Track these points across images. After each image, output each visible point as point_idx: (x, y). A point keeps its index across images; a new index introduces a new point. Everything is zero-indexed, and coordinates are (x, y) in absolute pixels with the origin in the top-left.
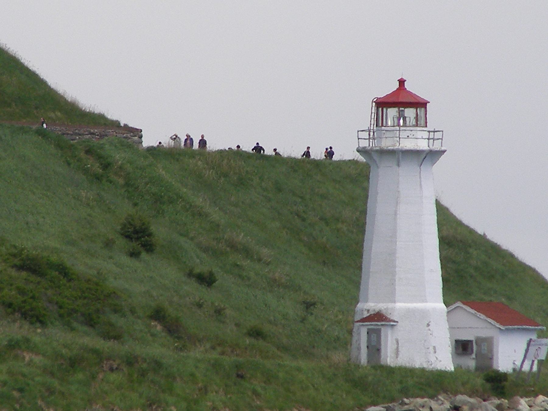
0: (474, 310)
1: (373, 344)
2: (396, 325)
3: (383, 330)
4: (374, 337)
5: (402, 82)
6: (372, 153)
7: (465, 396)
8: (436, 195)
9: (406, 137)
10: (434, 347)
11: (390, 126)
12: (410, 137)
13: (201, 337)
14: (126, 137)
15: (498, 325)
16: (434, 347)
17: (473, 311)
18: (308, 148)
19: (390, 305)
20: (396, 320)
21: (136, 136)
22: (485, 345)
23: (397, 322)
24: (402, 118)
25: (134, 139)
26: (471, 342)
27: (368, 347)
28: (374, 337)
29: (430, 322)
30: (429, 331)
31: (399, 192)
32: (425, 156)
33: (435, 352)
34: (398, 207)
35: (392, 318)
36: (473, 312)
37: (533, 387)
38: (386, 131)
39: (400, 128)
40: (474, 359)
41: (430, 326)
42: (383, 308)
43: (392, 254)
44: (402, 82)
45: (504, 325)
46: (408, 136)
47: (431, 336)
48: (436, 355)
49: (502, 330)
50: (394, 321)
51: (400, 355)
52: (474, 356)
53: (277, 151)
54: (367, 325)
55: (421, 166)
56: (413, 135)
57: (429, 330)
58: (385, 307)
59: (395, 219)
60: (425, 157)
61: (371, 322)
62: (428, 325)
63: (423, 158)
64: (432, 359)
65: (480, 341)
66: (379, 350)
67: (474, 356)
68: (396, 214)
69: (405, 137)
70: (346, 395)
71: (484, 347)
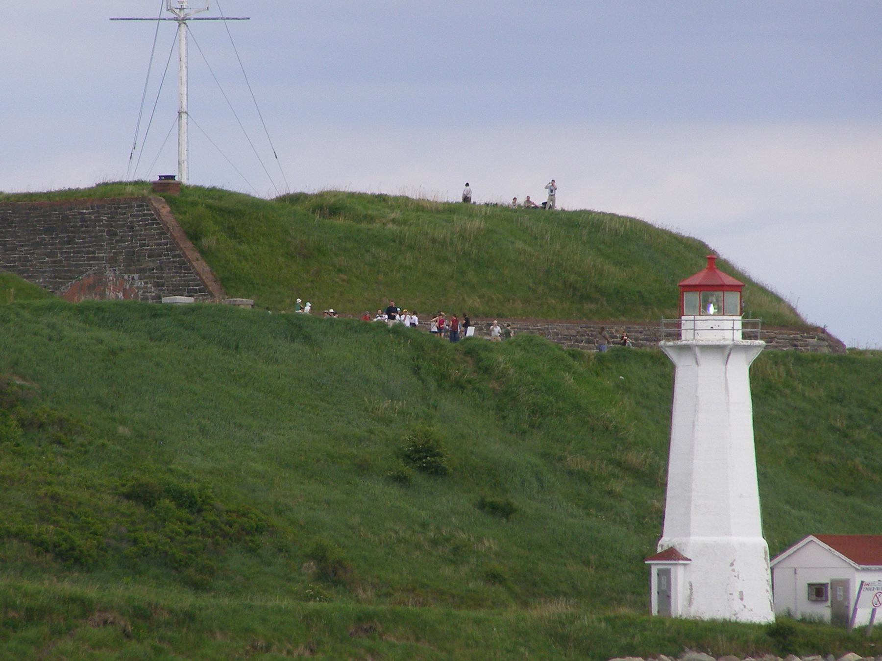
0: (827, 546)
1: (664, 588)
3: (673, 569)
4: (664, 578)
5: (528, 197)
6: (667, 349)
7: (703, 653)
10: (741, 593)
11: (712, 314)
13: (124, 578)
14: (794, 338)
15: (852, 563)
16: (741, 593)
17: (827, 547)
20: (689, 558)
21: (813, 338)
23: (690, 560)
26: (825, 585)
27: (658, 593)
28: (664, 578)
30: (734, 573)
31: (697, 397)
32: (729, 352)
33: (742, 599)
36: (827, 548)
37: (875, 643)
38: (686, 320)
40: (828, 606)
42: (676, 544)
44: (528, 197)
45: (859, 564)
46: (712, 327)
47: (736, 578)
48: (744, 602)
49: (859, 569)
50: (687, 559)
51: (695, 602)
52: (829, 603)
54: (657, 564)
56: (719, 326)
57: (733, 570)
61: (868, 565)
62: (732, 564)
63: (727, 355)
65: (835, 583)
66: (669, 597)
70: (529, 654)
71: (840, 593)
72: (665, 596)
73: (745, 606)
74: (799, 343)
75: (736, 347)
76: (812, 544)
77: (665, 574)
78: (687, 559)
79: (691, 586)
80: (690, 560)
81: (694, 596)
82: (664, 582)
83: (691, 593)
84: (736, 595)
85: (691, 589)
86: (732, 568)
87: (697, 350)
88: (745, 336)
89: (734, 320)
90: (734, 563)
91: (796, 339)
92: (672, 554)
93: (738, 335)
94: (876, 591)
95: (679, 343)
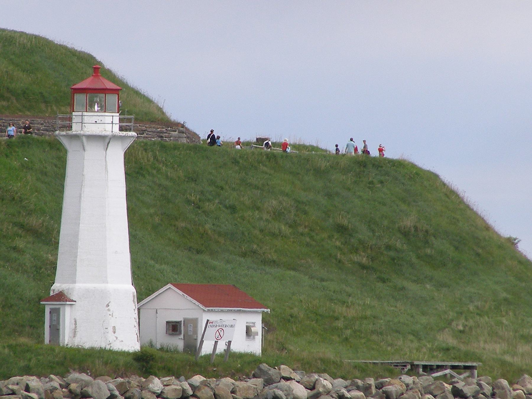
1: (54, 323)
2: (74, 304)
8: (187, 182)
9: (94, 122)
12: (98, 122)
18: (337, 146)
19: (71, 286)
22: (191, 326)
23: (75, 301)
24: (96, 104)
25: (172, 134)
26: (180, 322)
27: (246, 332)
29: (110, 302)
33: (114, 332)
34: (83, 189)
35: (71, 298)
39: (82, 114)
40: (182, 339)
41: (110, 306)
43: (76, 236)
45: (206, 307)
46: (96, 122)
48: (116, 335)
50: (73, 301)
51: (78, 335)
53: (338, 147)
55: (107, 151)
56: (101, 121)
57: (109, 310)
58: (67, 287)
59: (80, 202)
60: (109, 142)
62: (108, 306)
64: (111, 337)
66: (58, 330)
67: (182, 336)
68: (80, 197)
69: (93, 122)
71: (191, 329)
72: (55, 330)
73: (117, 338)
74: (164, 135)
75: (114, 137)
76: (169, 292)
77: (55, 312)
78: (73, 301)
79: (76, 321)
80: (75, 301)
81: (78, 330)
82: (55, 318)
83: (76, 327)
84: (110, 330)
85: (76, 324)
86: (107, 308)
87: (84, 139)
88: (121, 129)
89: (113, 116)
90: (109, 304)
91: (162, 132)
92: (61, 297)
93: (116, 128)
94: (218, 328)
95: (70, 132)
